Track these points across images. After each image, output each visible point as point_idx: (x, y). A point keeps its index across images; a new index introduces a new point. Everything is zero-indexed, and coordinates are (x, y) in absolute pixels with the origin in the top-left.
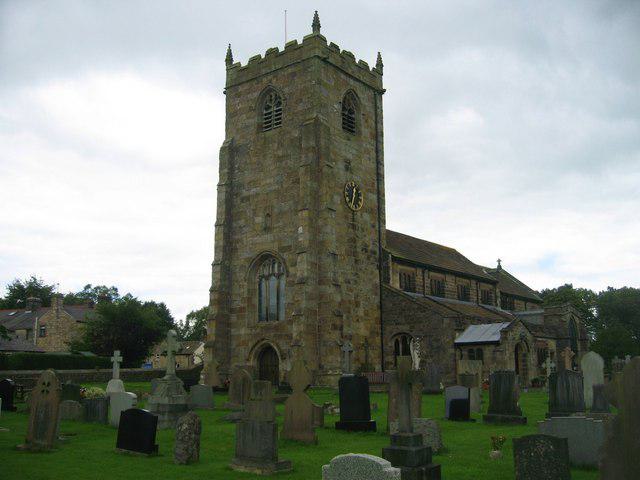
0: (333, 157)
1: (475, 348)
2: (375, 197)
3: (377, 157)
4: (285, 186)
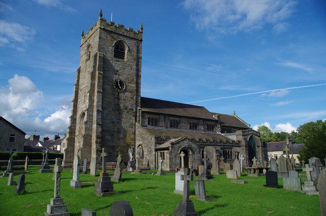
1: (162, 152)
2: (134, 85)
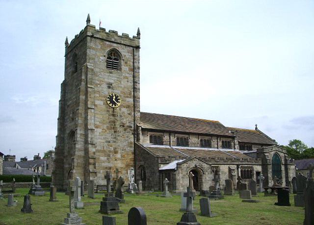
2: (132, 100)
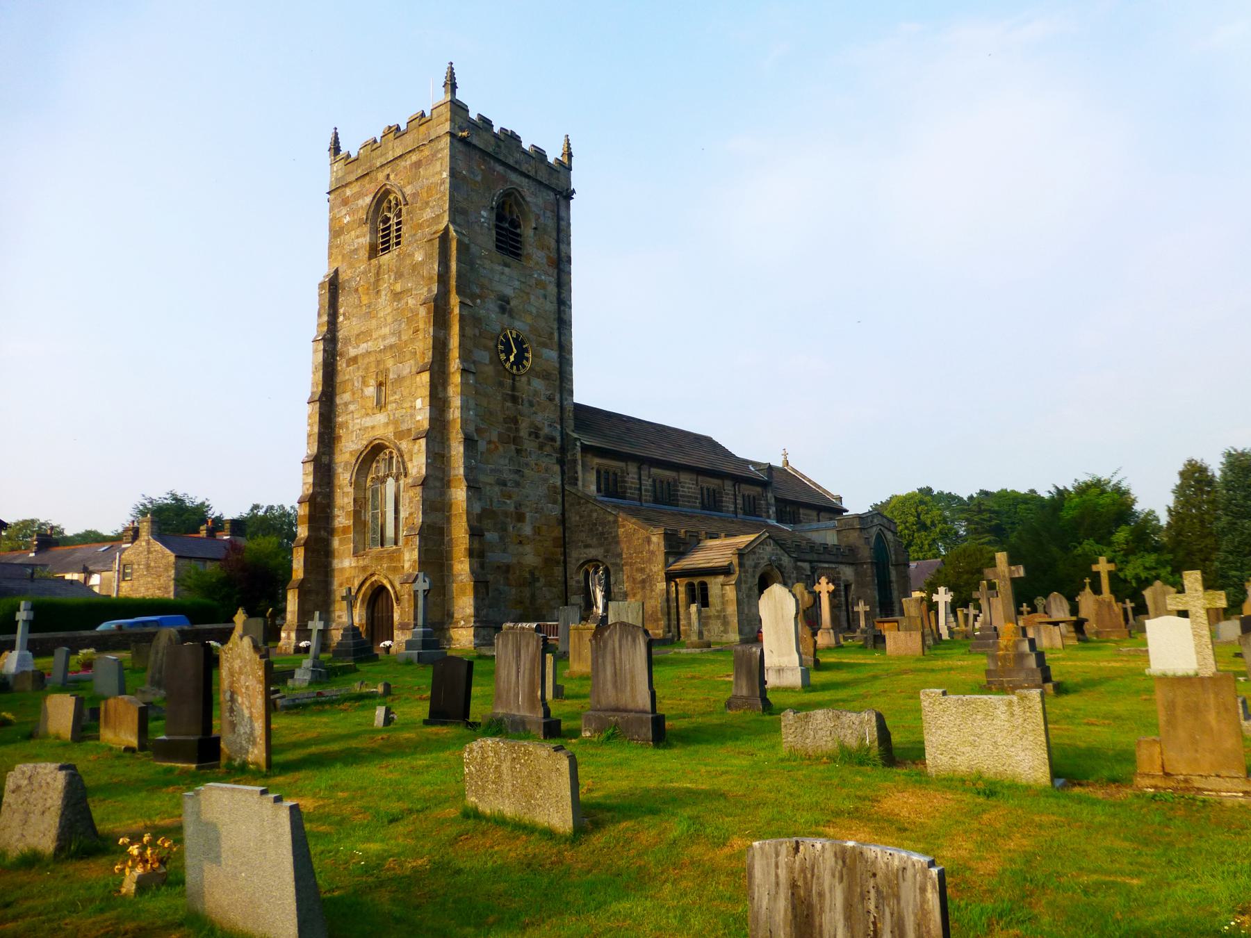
0: (478, 291)
1: (696, 581)
2: (553, 354)
3: (559, 293)
4: (404, 338)
